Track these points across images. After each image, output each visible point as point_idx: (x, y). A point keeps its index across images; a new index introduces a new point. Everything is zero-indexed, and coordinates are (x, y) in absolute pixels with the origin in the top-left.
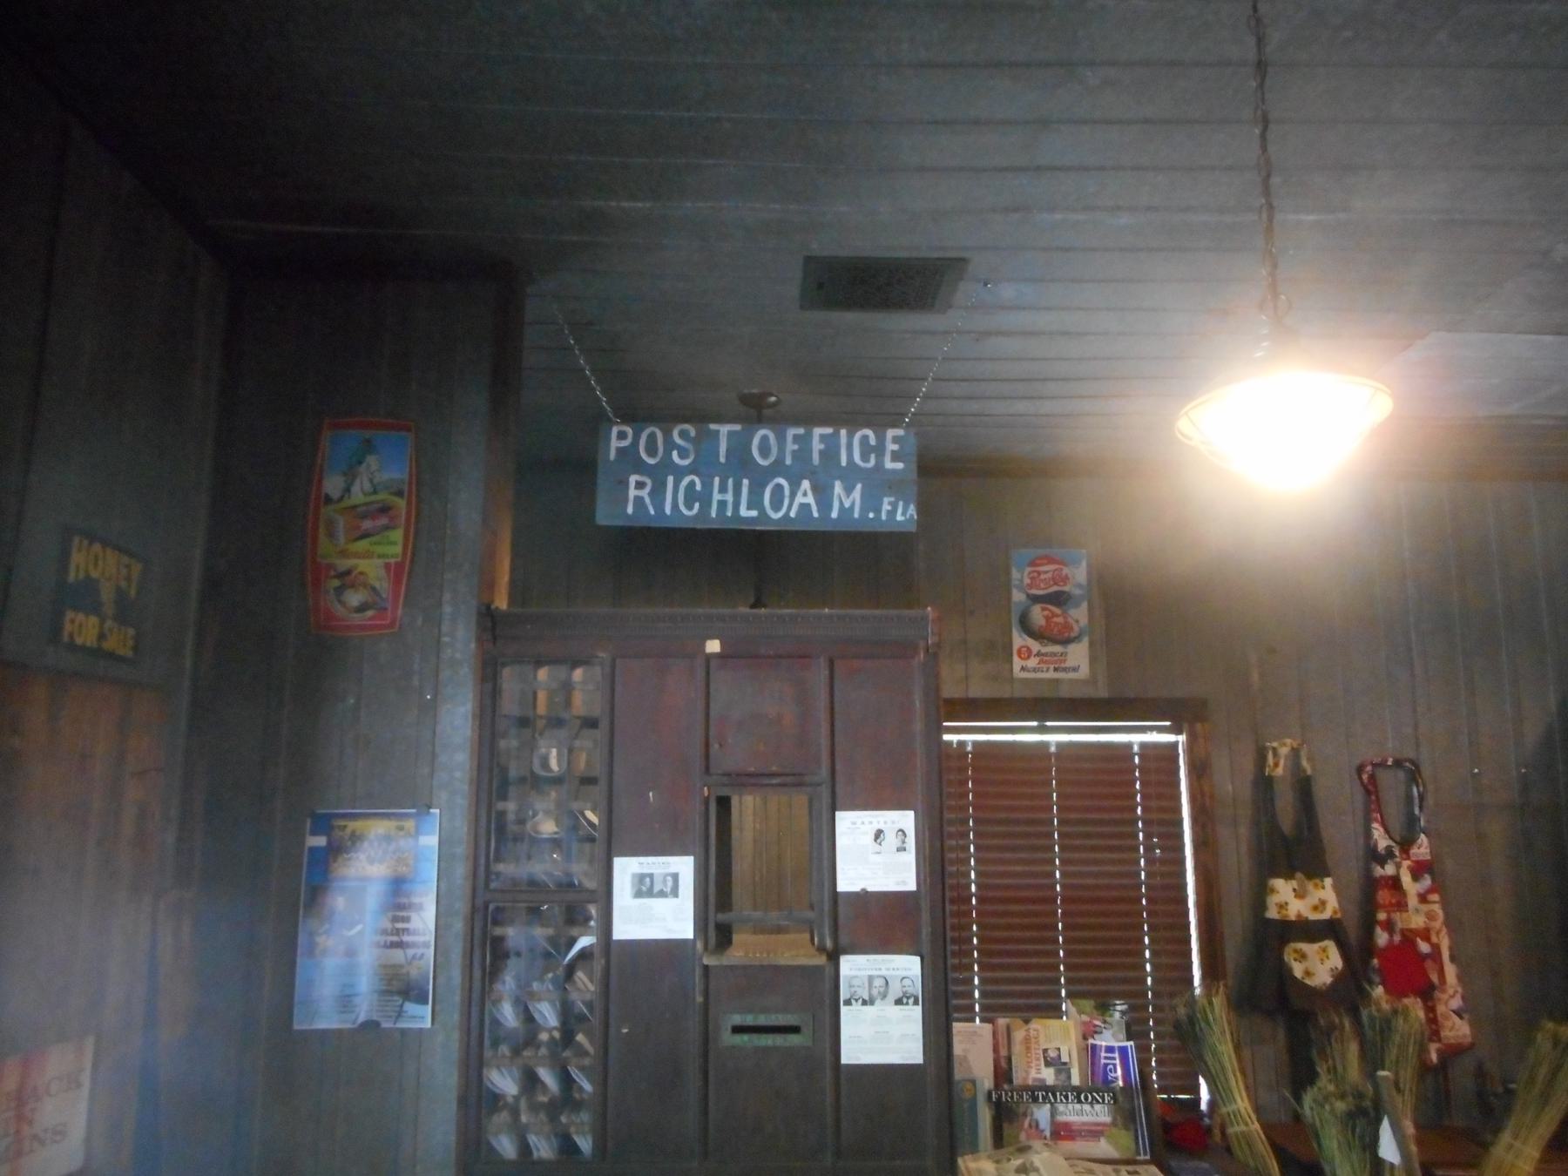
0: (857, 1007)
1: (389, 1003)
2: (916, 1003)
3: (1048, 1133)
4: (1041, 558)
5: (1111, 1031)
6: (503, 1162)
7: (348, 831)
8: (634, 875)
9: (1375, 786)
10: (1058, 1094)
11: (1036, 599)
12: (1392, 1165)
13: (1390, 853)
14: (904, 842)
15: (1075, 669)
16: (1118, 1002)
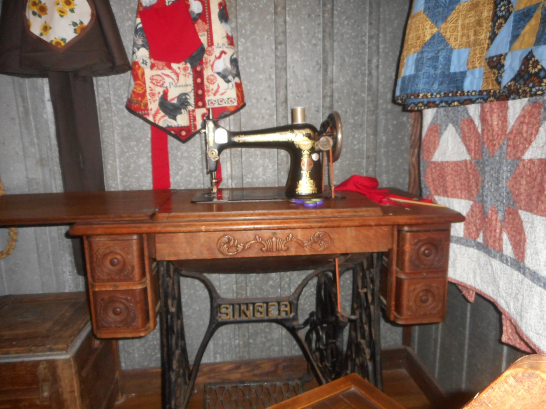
12: (439, 195)
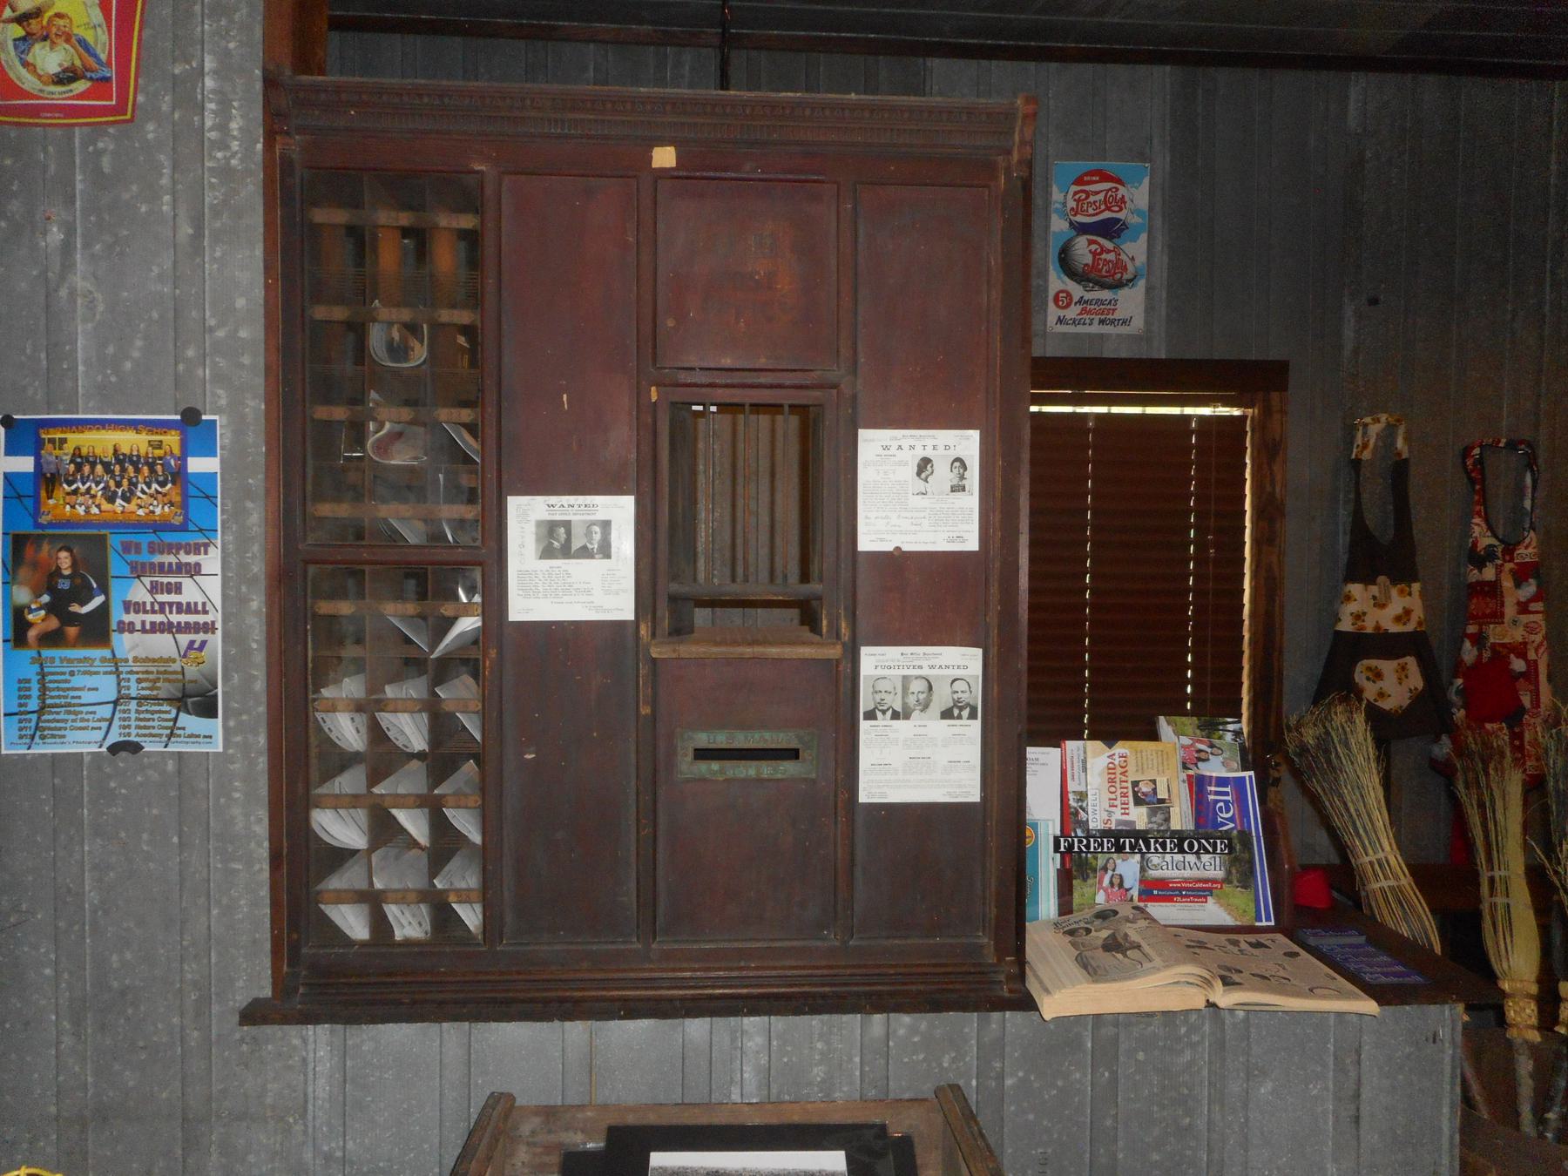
0: (883, 721)
1: (156, 716)
2: (973, 716)
3: (1135, 893)
4: (1091, 173)
5: (1221, 758)
6: (348, 942)
7: (69, 448)
8: (539, 524)
9: (1482, 472)
10: (1152, 841)
11: (1082, 229)
13: (1490, 555)
14: (962, 477)
15: (1125, 322)
16: (1229, 720)
